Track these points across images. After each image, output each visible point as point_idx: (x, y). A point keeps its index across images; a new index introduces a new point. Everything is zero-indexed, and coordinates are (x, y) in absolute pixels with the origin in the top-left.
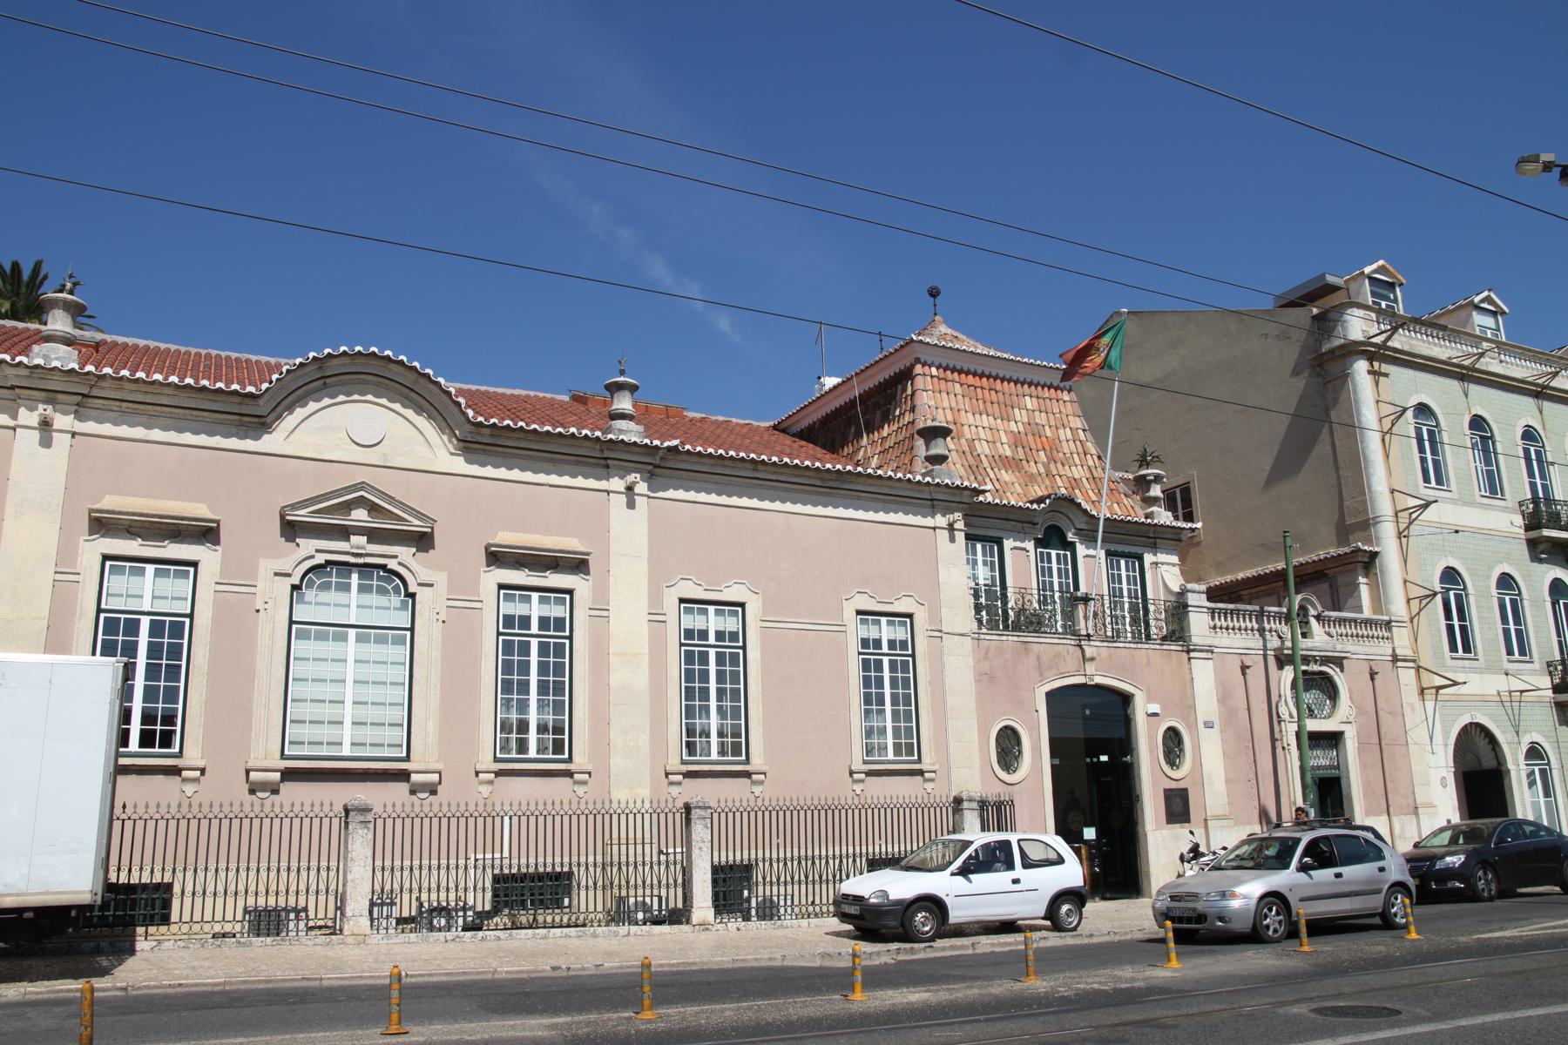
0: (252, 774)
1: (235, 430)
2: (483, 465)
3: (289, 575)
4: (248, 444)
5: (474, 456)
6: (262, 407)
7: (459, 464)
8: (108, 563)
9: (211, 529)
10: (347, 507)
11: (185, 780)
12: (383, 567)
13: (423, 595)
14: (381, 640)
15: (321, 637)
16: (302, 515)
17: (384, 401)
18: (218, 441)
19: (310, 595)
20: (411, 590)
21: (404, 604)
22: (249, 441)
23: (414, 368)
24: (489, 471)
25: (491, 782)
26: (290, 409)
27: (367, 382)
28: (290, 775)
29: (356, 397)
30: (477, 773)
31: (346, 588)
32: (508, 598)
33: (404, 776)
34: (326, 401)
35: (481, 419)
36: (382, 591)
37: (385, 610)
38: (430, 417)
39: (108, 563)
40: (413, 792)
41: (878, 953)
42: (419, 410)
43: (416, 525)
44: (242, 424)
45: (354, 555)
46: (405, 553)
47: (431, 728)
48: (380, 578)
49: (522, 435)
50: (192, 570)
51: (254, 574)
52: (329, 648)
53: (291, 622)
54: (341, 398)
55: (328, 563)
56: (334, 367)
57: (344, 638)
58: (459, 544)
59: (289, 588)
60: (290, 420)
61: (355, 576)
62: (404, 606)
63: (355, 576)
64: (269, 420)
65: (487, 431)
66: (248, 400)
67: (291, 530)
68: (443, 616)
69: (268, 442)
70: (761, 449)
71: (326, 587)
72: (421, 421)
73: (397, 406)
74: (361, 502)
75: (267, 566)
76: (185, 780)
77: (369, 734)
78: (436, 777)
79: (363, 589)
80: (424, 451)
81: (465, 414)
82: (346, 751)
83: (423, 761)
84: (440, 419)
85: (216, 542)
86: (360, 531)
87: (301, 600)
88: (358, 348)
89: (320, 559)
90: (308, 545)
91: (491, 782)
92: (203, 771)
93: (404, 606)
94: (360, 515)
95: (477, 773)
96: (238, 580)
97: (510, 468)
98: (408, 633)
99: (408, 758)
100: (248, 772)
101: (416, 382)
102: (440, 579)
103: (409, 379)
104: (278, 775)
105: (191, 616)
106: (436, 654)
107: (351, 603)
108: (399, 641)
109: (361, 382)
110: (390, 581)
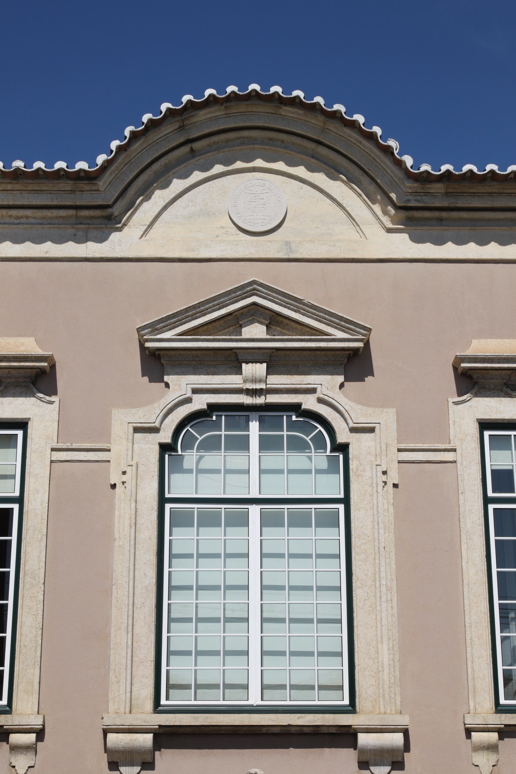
0: (110, 736)
1: (71, 231)
2: (439, 242)
3: (155, 430)
4: (91, 249)
6: (105, 191)
7: (402, 245)
9: (42, 372)
10: (234, 322)
11: (15, 749)
12: (296, 408)
13: (360, 446)
14: (300, 521)
15: (209, 521)
16: (169, 339)
17: (280, 166)
18: (49, 249)
19: (190, 458)
20: (341, 439)
21: (333, 461)
22: (91, 245)
23: (315, 107)
24: (450, 250)
25: (492, 748)
26: (146, 192)
27: (253, 141)
28: (168, 738)
29: (239, 165)
30: (468, 732)
31: (243, 444)
32: (499, 443)
33: (345, 737)
34: (197, 176)
35: (425, 167)
36: (298, 445)
37: (303, 473)
38: (351, 180)
40: (363, 765)
41: (216, 118)
42: (333, 172)
43: (339, 338)
44: (79, 221)
46: (327, 384)
47: (385, 656)
48: (292, 426)
49: (495, 187)
50: (20, 433)
51: (105, 433)
52: (212, 538)
53: (162, 500)
54: (218, 169)
55: (213, 408)
56: (204, 121)
57: (243, 521)
58: (412, 361)
59: (156, 449)
60: (147, 210)
61: (254, 426)
62: (332, 469)
63: (254, 426)
64: (116, 210)
65: (438, 188)
66: (83, 185)
67: (157, 364)
68: (393, 477)
69: (121, 242)
71: (212, 445)
72: (338, 188)
73: (301, 171)
74: (254, 313)
75: (122, 420)
76: (15, 749)
77: (280, 670)
78: (398, 739)
79: (267, 444)
80: (347, 231)
81: (400, 164)
82: (254, 699)
83: (379, 710)
84: (365, 180)
86: (255, 355)
87: (178, 467)
88: (231, 89)
89: (200, 402)
90: (181, 384)
91: (492, 748)
92: (40, 734)
93: (332, 469)
94: (255, 331)
95: (468, 732)
96: (82, 445)
97: (482, 242)
98: (341, 507)
99: (352, 708)
100: (105, 732)
101: (323, 130)
102: (386, 419)
103: (312, 126)
104: (149, 738)
105: (20, 500)
106: (387, 538)
107: (250, 467)
108: (328, 521)
109: (244, 142)
110: (307, 429)
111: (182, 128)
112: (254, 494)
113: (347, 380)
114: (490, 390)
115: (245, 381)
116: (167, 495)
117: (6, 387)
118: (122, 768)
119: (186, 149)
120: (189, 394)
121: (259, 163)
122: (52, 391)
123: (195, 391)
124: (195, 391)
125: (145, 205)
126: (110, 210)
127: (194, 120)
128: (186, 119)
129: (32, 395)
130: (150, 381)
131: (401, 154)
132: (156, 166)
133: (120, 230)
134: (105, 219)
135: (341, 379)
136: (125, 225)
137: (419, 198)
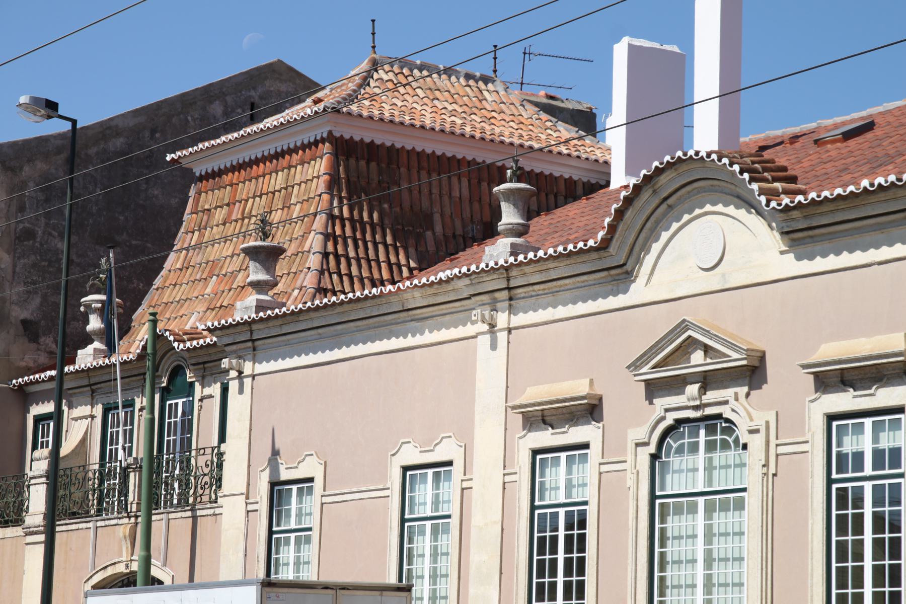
3: (646, 444)
5: (809, 248)
7: (791, 265)
8: (835, 424)
19: (675, 461)
26: (646, 248)
31: (694, 448)
34: (675, 226)
39: (835, 424)
43: (736, 359)
45: (696, 408)
55: (679, 422)
57: (693, 509)
64: (628, 267)
69: (638, 291)
70: (186, 355)
79: (711, 446)
85: (599, 419)
111: (655, 192)
112: (700, 488)
113: (751, 389)
114: (833, 387)
115: (689, 400)
116: (658, 493)
117: (578, 419)
118: (221, 575)
119: (664, 206)
120: (663, 414)
121: (708, 208)
122: (599, 419)
123: (667, 410)
124: (667, 410)
125: (647, 257)
126: (625, 267)
127: (659, 184)
128: (655, 184)
129: (589, 423)
130: (766, 383)
131: (759, 195)
132: (649, 225)
133: (634, 281)
134: (621, 275)
135: (745, 389)
136: (636, 277)
137: (789, 224)
